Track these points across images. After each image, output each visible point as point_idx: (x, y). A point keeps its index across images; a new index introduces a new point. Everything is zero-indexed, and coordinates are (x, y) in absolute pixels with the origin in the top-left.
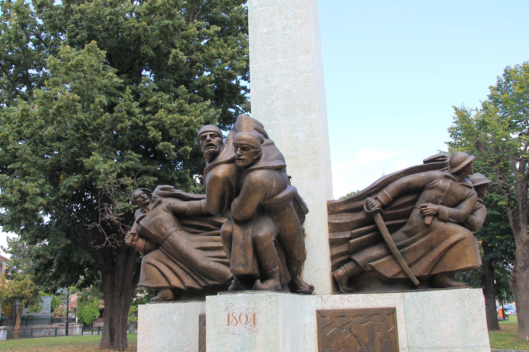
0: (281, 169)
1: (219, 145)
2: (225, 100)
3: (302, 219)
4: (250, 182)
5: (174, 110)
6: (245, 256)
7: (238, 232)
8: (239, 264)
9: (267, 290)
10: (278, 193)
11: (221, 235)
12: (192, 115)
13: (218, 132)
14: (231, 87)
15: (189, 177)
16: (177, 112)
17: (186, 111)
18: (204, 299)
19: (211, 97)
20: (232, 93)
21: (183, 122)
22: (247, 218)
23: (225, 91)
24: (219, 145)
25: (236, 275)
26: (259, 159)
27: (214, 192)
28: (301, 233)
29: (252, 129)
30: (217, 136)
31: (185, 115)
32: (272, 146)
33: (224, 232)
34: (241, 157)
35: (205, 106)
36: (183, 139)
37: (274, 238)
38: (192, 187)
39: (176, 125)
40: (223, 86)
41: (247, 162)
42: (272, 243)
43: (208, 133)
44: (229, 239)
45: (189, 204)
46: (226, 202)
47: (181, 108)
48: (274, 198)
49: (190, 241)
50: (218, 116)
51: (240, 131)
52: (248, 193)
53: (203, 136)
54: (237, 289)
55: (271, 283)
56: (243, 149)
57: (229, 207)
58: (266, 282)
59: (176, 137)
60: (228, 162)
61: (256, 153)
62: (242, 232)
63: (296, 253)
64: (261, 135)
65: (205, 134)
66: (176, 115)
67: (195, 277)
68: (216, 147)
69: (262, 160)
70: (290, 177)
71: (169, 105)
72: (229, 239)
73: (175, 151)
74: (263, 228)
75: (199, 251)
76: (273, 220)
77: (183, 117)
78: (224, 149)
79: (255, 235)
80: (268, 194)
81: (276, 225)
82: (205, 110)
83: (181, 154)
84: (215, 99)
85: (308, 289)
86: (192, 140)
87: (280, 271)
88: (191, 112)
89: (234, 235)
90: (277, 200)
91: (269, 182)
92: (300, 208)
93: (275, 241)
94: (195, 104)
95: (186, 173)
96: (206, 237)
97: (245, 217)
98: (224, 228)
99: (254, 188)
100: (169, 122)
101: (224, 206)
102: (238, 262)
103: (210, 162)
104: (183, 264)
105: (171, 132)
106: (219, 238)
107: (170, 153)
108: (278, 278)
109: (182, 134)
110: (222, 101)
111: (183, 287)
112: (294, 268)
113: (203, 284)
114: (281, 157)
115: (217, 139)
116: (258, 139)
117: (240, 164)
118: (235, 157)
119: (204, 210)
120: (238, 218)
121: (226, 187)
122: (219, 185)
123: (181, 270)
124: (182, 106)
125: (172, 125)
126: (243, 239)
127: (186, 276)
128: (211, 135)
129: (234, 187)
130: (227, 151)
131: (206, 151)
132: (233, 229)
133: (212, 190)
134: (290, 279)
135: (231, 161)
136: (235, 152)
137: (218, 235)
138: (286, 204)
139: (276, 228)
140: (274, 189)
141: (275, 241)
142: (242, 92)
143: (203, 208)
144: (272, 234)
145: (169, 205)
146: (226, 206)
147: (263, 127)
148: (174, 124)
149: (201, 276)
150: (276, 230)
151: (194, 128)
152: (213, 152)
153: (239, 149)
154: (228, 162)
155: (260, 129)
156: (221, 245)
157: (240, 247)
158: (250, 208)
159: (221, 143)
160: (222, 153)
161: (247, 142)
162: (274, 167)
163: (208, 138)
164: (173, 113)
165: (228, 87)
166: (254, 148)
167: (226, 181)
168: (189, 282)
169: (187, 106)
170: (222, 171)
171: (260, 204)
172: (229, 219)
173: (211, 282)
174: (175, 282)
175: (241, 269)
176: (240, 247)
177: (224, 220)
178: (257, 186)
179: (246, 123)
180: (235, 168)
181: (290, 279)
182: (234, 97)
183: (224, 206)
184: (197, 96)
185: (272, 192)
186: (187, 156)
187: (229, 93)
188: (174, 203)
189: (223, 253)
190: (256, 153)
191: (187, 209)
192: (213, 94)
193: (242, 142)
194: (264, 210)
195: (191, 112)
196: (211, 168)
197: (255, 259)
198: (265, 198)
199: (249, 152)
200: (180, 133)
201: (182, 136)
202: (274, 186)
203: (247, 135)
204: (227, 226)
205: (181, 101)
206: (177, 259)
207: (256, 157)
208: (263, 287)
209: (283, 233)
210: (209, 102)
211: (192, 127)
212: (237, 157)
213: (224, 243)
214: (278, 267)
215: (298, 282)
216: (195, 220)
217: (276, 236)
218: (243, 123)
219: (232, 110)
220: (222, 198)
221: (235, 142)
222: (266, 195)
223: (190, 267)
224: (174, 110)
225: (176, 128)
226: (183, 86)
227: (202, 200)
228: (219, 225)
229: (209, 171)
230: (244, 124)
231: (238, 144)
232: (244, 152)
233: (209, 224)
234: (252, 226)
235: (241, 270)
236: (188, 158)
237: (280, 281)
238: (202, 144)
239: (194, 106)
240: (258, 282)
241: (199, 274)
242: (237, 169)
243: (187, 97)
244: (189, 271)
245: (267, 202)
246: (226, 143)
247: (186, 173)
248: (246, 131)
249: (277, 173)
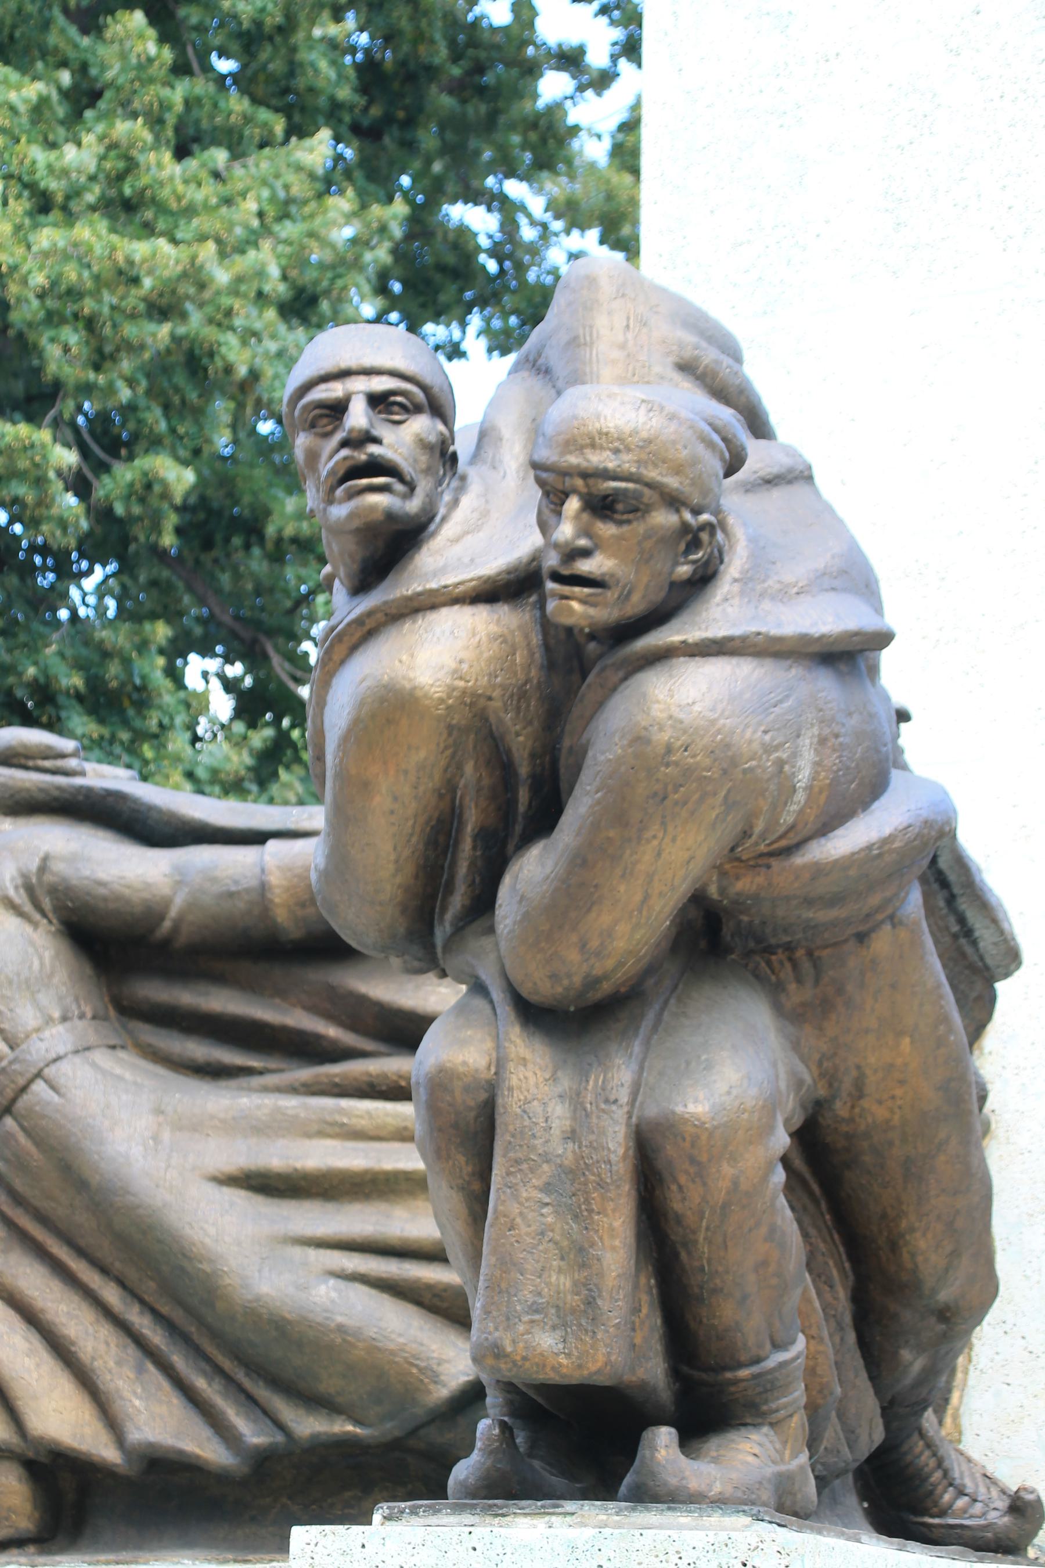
0: (849, 657)
1: (428, 471)
2: (428, 138)
3: (978, 1009)
4: (640, 740)
5: (75, 193)
6: (580, 1256)
7: (535, 1083)
8: (535, 1309)
9: (721, 1503)
10: (826, 827)
11: (420, 1093)
12: (202, 238)
13: (428, 379)
14: (474, 42)
15: (158, 678)
16: (93, 208)
17: (162, 208)
18: (283, 1547)
19: (334, 113)
20: (482, 91)
21: (136, 281)
22: (606, 988)
23: (431, 72)
24: (428, 471)
25: (509, 1387)
26: (704, 579)
27: (381, 800)
28: (963, 1105)
29: (662, 366)
30: (418, 409)
31: (148, 230)
32: (799, 490)
33: (441, 1082)
34: (586, 567)
35: (291, 177)
36: (130, 409)
37: (781, 1140)
38: (178, 742)
39: (88, 306)
40: (420, 37)
41: (625, 597)
42: (769, 1170)
43: (360, 385)
44: (472, 1134)
45: (177, 869)
46: (463, 869)
47: (121, 177)
48: (799, 860)
49: (178, 1126)
50: (381, 254)
51: (577, 379)
52: (622, 819)
53: (321, 405)
54: (508, 1488)
55: (749, 1454)
56: (602, 506)
57: (483, 904)
58: (713, 1445)
59: (87, 389)
60: (489, 593)
61: (691, 538)
62: (565, 1083)
63: (925, 1248)
64: (726, 414)
65: (335, 390)
66: (92, 233)
67: (200, 1383)
68: (411, 487)
69: (724, 587)
70: (903, 716)
71: (38, 155)
72: (472, 1134)
73: (80, 486)
74: (709, 1067)
75: (239, 1197)
76: (778, 1009)
77: (140, 249)
78: (467, 502)
79: (652, 1111)
80: (759, 826)
81: (796, 1046)
82: (285, 210)
83: (119, 509)
84: (357, 130)
85: (998, 1518)
86: (198, 413)
87: (811, 1372)
88: (190, 211)
89: (511, 1105)
90: (819, 870)
91: (768, 749)
92: (968, 932)
93: (785, 1160)
94: (220, 156)
95: (143, 646)
96: (291, 1103)
97: (592, 982)
98: (436, 1050)
99: (665, 780)
100: (39, 279)
101: (446, 895)
102: (527, 1295)
103: (361, 587)
104: (122, 1283)
105: (53, 351)
106: (404, 1111)
107: (44, 501)
108: (798, 1422)
109: (126, 365)
110: (409, 146)
111: (109, 1453)
112: (906, 1354)
113: (254, 1435)
114: (856, 578)
115: (421, 425)
116: (710, 445)
117: (577, 609)
118: (536, 557)
119: (281, 916)
120: (541, 986)
121: (469, 768)
122: (421, 754)
123: (105, 1331)
124: (131, 166)
125: (63, 303)
126: (572, 1136)
127: (140, 1370)
128: (377, 401)
129: (524, 770)
130: (485, 514)
131: (339, 511)
132: (500, 1063)
133: (366, 786)
134: (873, 1434)
135: (515, 587)
136: (544, 527)
137: (398, 1092)
138: (875, 900)
139: (801, 1068)
140: (800, 797)
141: (785, 1160)
142: (553, 86)
143: (278, 897)
144: (770, 1108)
145: (43, 869)
146: (458, 901)
147: (737, 357)
148: (73, 294)
149: (240, 1376)
150: (799, 1083)
151: (210, 333)
152: (390, 516)
153: (573, 504)
154: (489, 593)
155: (716, 376)
156: (408, 1159)
157: (547, 1188)
158: (630, 924)
159: (444, 455)
160: (448, 530)
161: (626, 463)
162: (805, 639)
163: (358, 416)
164: (70, 217)
165: (452, 43)
166: (674, 501)
167: (472, 724)
168: (158, 1419)
169: (162, 169)
170: (443, 653)
171: (698, 898)
172: (479, 988)
173: (309, 1425)
174: (58, 1415)
175: (547, 1341)
176: (547, 1188)
177: (436, 995)
178: (688, 772)
179: (619, 322)
180: (536, 639)
181: (879, 1435)
182: (489, 124)
183: (446, 895)
184: (237, 104)
185: (787, 818)
186: (156, 527)
187: (459, 89)
188: (73, 858)
189: (415, 1222)
190: (691, 538)
191: (167, 902)
192: (344, 93)
193: (598, 459)
194: (711, 940)
195: (190, 211)
196: (364, 633)
197: (648, 1281)
198: (735, 857)
199: (639, 528)
200: (113, 358)
201: (131, 382)
202: (803, 775)
203: (627, 407)
204: (460, 1037)
205: (122, 128)
206: (81, 1252)
207: (684, 570)
208: (694, 1484)
209: (841, 1108)
210: (319, 149)
211: (196, 318)
212: (552, 560)
213: (436, 1154)
214: (801, 1339)
215: (926, 1459)
216: (220, 980)
217: (798, 1122)
218: (601, 322)
219: (479, 221)
220: (440, 835)
221: (546, 455)
222: (746, 834)
223: (165, 1309)
224: (75, 193)
225: (90, 324)
226: (138, 18)
227: (272, 845)
228: (405, 1031)
229: (354, 648)
230: (608, 329)
231: (565, 473)
232: (607, 530)
233: (313, 1009)
234: (637, 1047)
235: (552, 1351)
236: (168, 540)
237: (812, 1443)
238: (313, 457)
239: (216, 175)
240: (663, 1441)
241: (227, 1364)
242: (547, 647)
243: (165, 106)
244: (156, 1336)
245: (745, 884)
246: (476, 457)
247: (143, 646)
248: (623, 381)
249: (825, 686)
